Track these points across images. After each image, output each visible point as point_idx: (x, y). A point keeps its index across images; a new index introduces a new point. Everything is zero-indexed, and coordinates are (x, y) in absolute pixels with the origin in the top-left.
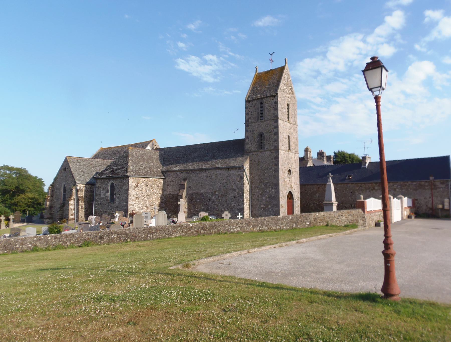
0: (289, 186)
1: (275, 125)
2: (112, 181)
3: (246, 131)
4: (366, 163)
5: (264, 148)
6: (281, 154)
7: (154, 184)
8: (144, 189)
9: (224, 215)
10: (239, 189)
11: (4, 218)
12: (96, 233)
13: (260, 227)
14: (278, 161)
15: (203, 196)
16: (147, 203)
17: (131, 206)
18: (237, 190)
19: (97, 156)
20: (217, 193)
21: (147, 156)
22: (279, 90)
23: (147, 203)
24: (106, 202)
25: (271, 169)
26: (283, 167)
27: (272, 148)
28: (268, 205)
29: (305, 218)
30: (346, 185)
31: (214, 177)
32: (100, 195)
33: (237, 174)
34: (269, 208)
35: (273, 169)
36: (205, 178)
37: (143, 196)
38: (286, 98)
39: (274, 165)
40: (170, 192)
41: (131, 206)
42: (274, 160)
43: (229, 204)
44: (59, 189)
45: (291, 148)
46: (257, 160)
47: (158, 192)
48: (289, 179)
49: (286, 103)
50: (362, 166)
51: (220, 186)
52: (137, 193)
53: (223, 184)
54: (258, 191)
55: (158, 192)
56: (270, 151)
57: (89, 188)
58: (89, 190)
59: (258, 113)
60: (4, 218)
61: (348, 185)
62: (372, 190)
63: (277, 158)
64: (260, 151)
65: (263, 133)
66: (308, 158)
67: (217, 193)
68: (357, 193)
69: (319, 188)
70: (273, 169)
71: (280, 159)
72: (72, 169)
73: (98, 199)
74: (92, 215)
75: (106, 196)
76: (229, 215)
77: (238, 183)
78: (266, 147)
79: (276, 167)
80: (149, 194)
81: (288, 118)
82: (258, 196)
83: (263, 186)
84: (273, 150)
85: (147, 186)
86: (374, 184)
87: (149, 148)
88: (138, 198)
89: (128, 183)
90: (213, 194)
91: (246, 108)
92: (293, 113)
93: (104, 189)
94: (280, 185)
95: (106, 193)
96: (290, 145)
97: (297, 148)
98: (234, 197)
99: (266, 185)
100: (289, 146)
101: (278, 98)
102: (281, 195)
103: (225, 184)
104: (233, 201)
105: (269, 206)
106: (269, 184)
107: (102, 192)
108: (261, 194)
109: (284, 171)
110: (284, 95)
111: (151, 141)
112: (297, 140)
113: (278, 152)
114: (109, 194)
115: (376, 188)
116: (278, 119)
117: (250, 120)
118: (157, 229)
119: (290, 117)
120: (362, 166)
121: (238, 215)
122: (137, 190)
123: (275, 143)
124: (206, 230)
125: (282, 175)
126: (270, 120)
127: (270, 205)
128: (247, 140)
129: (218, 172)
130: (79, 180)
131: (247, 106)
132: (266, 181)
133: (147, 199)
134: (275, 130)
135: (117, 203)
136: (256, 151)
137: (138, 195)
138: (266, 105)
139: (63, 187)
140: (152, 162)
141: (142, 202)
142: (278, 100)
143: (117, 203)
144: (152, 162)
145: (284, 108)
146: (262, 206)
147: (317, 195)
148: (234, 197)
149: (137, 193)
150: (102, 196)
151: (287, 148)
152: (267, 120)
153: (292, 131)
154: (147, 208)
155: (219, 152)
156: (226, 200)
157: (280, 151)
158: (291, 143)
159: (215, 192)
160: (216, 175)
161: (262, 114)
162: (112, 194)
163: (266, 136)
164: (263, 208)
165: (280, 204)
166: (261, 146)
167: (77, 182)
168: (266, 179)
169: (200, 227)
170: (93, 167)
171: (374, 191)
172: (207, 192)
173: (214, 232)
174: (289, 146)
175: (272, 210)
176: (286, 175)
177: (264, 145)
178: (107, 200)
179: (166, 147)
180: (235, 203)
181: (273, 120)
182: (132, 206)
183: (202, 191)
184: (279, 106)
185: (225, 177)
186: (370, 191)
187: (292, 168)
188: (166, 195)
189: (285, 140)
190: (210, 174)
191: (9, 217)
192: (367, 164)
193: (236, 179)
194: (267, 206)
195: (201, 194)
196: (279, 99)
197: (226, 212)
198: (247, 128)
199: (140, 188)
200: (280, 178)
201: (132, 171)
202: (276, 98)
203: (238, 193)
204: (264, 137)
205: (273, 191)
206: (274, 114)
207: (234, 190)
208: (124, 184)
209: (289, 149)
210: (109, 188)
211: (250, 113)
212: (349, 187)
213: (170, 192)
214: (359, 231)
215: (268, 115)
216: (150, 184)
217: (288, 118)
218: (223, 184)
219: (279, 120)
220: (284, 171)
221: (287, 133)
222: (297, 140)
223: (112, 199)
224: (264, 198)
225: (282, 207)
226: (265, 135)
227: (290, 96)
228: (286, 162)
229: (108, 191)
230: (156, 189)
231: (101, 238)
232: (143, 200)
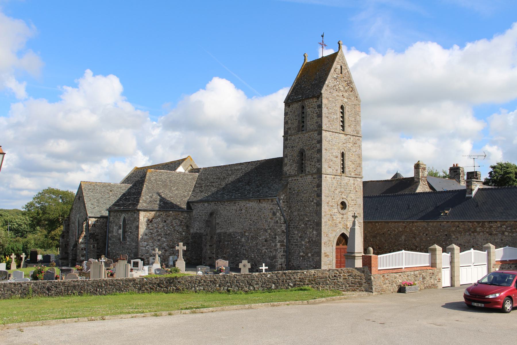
0: (341, 226)
1: (318, 137)
2: (124, 215)
3: (285, 147)
4: (472, 190)
5: (305, 170)
6: (170, 197)
7: (175, 219)
8: (161, 226)
9: (241, 266)
10: (270, 229)
11: (15, 256)
12: (44, 283)
13: (228, 287)
14: (321, 191)
15: (232, 238)
16: (165, 245)
17: (141, 248)
18: (269, 231)
19: (123, 182)
20: (247, 234)
21: (170, 181)
22: (325, 87)
23: (165, 245)
24: (118, 241)
25: (312, 201)
26: (330, 199)
27: (314, 172)
28: (308, 253)
29: (288, 278)
30: (439, 224)
31: (243, 211)
32: (113, 231)
33: (270, 208)
34: (309, 258)
35: (315, 201)
36: (234, 212)
37: (159, 235)
38: (337, 98)
39: (316, 196)
40: (197, 229)
41: (141, 248)
42: (316, 189)
43: (259, 249)
44: (74, 223)
45: (347, 170)
46: (296, 188)
47: (181, 230)
48: (341, 216)
49: (339, 106)
50: (467, 196)
51: (251, 225)
52: (151, 231)
53: (254, 221)
54: (296, 232)
55: (181, 230)
56: (312, 175)
57: (104, 223)
58: (34, 232)
59: (299, 122)
60: (15, 256)
61: (443, 224)
62: (473, 232)
63: (319, 186)
64: (300, 175)
65: (303, 150)
66: (419, 179)
67: (247, 234)
68: (454, 237)
69: (405, 227)
70: (315, 201)
71: (323, 188)
72: (85, 198)
73: (111, 237)
74: (183, 251)
75: (118, 234)
76: (249, 266)
77: (270, 220)
78: (307, 170)
79: (318, 199)
80: (169, 232)
81: (343, 126)
82: (297, 240)
83: (303, 225)
84: (315, 174)
85: (165, 222)
86: (475, 223)
87: (181, 169)
88: (153, 238)
89: (139, 218)
90: (243, 235)
91: (286, 114)
92: (353, 119)
93: (116, 225)
94: (323, 224)
95: (118, 230)
96: (346, 165)
97: (358, 171)
98: (266, 241)
99: (306, 224)
100: (343, 168)
101: (322, 100)
102: (324, 239)
103: (255, 221)
104: (264, 246)
105: (310, 255)
106: (309, 223)
107: (115, 228)
108: (300, 237)
109: (330, 204)
110: (335, 94)
111: (183, 160)
112: (359, 157)
113: (321, 177)
114: (121, 231)
115: (478, 229)
116: (322, 130)
117: (289, 132)
118: (107, 283)
119: (346, 125)
120: (467, 196)
121: (266, 266)
122: (151, 228)
123: (317, 165)
124: (162, 287)
125: (327, 210)
126: (312, 131)
127: (311, 252)
128: (286, 159)
129: (248, 205)
130: (91, 212)
131: (287, 111)
132: (307, 219)
133: (164, 239)
134: (318, 145)
135: (128, 243)
136: (296, 176)
137: (152, 233)
138: (309, 110)
139: (77, 220)
140: (177, 189)
141: (158, 243)
142: (322, 102)
143: (128, 243)
144: (177, 189)
145: (335, 113)
146: (302, 254)
147: (403, 237)
148: (266, 241)
149: (151, 231)
150: (114, 234)
151: (340, 170)
152: (309, 132)
153: (349, 145)
154: (166, 251)
155: (257, 176)
156: (257, 244)
157: (323, 176)
158: (347, 163)
159: (245, 232)
160: (246, 208)
161: (303, 122)
162: (124, 232)
163: (308, 153)
164: (302, 256)
165: (323, 251)
166: (301, 169)
167: (89, 215)
168: (306, 215)
169: (155, 283)
170: (113, 195)
171: (476, 234)
172: (236, 232)
173: (172, 290)
174: (343, 168)
175: (313, 260)
176: (337, 209)
177: (305, 166)
178: (120, 239)
179: (234, 163)
180: (267, 249)
181: (316, 130)
182: (144, 249)
183: (231, 231)
184: (324, 110)
185: (255, 212)
186: (470, 234)
187: (349, 199)
188: (192, 234)
189: (334, 159)
190: (240, 207)
191: (21, 256)
192: (474, 193)
193: (268, 215)
194: (307, 254)
195: (230, 235)
196: (324, 101)
197: (245, 262)
198: (286, 143)
199: (155, 225)
200: (323, 214)
201: (145, 202)
202: (320, 99)
203: (270, 234)
204: (305, 155)
205: (315, 232)
206: (317, 123)
207: (266, 231)
208: (135, 219)
209: (343, 172)
210: (121, 223)
211: (289, 121)
212: (444, 226)
213: (197, 229)
214: (345, 298)
215: (310, 124)
216: (170, 219)
217: (343, 126)
218: (254, 221)
219: (323, 132)
220: (330, 204)
221: (339, 149)
222: (359, 157)
223: (124, 238)
224: (303, 243)
225: (327, 256)
226: (307, 152)
227: (346, 94)
228: (337, 192)
229: (120, 229)
230: (178, 226)
231: (48, 289)
232: (159, 240)
